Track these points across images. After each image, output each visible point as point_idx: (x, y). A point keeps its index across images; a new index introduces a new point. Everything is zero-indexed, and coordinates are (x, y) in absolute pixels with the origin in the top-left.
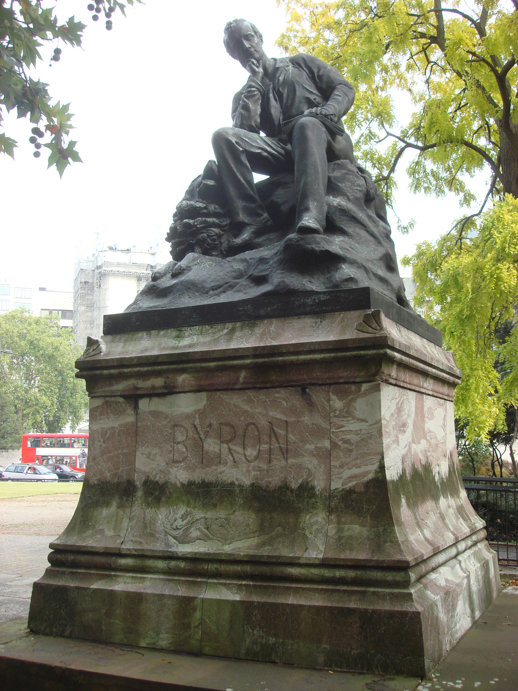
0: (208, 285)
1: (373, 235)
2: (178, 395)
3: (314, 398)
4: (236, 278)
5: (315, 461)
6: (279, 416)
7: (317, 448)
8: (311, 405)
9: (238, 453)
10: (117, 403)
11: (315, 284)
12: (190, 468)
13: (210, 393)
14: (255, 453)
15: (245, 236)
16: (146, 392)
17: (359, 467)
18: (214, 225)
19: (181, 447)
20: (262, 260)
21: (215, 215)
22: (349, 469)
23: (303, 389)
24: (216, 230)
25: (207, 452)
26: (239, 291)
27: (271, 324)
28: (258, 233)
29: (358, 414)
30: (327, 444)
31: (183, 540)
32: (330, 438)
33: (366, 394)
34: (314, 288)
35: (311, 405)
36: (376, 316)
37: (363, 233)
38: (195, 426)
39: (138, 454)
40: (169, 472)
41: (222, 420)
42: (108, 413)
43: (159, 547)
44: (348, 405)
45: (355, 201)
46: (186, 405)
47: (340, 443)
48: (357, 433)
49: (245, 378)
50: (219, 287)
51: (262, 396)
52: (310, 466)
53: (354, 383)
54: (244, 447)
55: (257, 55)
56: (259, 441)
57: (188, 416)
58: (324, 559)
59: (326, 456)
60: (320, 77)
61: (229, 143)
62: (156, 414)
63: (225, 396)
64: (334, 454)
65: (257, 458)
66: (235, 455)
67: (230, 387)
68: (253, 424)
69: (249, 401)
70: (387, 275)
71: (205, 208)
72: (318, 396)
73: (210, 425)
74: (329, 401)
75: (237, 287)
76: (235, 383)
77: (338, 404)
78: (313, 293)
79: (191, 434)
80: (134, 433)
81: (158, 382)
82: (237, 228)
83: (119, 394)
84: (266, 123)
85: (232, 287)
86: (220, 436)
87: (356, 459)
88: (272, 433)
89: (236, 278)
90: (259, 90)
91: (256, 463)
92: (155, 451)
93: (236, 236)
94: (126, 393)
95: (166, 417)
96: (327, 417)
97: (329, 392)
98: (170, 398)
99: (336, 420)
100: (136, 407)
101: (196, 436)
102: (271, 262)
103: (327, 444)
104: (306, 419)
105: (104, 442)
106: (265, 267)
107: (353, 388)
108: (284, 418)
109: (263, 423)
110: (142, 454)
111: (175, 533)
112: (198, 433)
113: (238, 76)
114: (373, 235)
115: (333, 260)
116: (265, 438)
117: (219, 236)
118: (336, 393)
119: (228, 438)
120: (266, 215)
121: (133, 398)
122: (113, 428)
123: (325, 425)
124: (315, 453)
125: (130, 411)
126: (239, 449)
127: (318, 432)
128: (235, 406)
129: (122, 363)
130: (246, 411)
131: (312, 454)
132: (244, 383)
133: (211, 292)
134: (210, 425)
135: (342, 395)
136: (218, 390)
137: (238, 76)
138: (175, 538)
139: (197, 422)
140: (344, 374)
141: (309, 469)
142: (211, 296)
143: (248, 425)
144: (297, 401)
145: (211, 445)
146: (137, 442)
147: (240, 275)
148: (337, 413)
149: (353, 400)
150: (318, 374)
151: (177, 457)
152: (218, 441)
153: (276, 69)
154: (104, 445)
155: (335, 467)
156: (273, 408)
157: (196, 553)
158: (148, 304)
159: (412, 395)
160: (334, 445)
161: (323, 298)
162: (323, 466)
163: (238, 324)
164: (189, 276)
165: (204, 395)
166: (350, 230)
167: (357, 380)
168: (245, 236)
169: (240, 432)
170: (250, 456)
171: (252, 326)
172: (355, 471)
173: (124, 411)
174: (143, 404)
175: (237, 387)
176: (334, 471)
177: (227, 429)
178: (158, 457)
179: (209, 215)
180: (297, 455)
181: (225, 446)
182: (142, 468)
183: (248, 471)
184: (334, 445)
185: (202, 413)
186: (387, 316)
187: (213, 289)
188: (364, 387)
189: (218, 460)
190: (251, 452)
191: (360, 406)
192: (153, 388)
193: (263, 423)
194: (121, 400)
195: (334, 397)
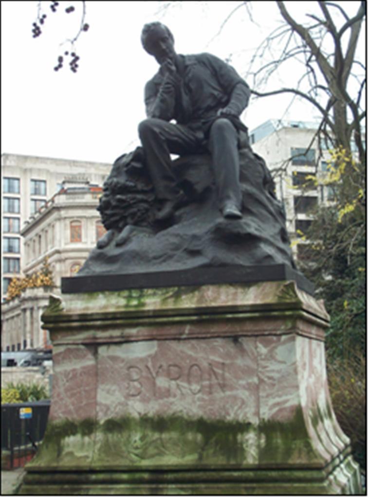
0: (151, 255)
1: (271, 213)
2: (135, 344)
3: (245, 346)
4: (173, 250)
5: (247, 393)
6: (217, 359)
7: (249, 384)
8: (243, 351)
9: (185, 388)
10: (78, 350)
11: (242, 259)
12: (145, 400)
13: (160, 342)
14: (198, 388)
15: (167, 210)
16: (105, 341)
17: (280, 396)
18: (142, 201)
19: (136, 384)
20: (195, 237)
21: (143, 192)
22: (274, 398)
23: (235, 339)
24: (145, 205)
25: (159, 388)
26: (178, 261)
27: (208, 289)
28: (177, 207)
29: (279, 358)
30: (255, 380)
31: (142, 457)
32: (258, 376)
33: (285, 342)
34: (241, 262)
35: (243, 351)
36: (291, 286)
37: (264, 212)
38: (147, 367)
39: (99, 391)
40: (127, 405)
41: (171, 363)
42: (70, 358)
43: (123, 463)
44: (271, 351)
45: (256, 185)
46: (140, 350)
47: (266, 379)
48: (278, 372)
49: (190, 330)
50: (160, 257)
51: (203, 344)
52: (243, 397)
53: (275, 335)
54: (189, 382)
55: (171, 55)
56: (201, 378)
57: (142, 360)
58: (259, 465)
59: (255, 389)
60: (222, 76)
61: (154, 132)
62: (114, 359)
63: (174, 345)
64: (261, 387)
65: (199, 391)
66: (183, 390)
67: (177, 337)
68: (196, 365)
69: (193, 347)
70: (282, 245)
71: (135, 186)
72: (248, 344)
73: (161, 367)
74: (256, 347)
75: (175, 258)
76: (181, 334)
77: (263, 350)
78: (241, 266)
79: (144, 374)
80: (96, 374)
81: (116, 333)
82: (160, 203)
83: (80, 342)
84: (178, 113)
85: (170, 257)
86: (168, 375)
87: (278, 391)
88: (212, 372)
89: (173, 250)
90: (173, 86)
91: (199, 395)
92: (114, 387)
93: (159, 210)
94: (87, 341)
95: (123, 361)
96: (255, 360)
97: (256, 341)
98: (124, 346)
99: (263, 363)
100: (95, 353)
101: (149, 376)
102: (203, 239)
103: (255, 380)
104: (239, 362)
105: (67, 381)
106: (198, 243)
107: (275, 338)
108: (221, 360)
109: (205, 364)
110: (103, 390)
111: (137, 452)
112: (151, 373)
113: (151, 67)
114: (271, 213)
115: (253, 240)
116: (206, 376)
117: (147, 210)
118: (261, 342)
119: (177, 376)
120: (182, 192)
121: (93, 346)
122: (74, 370)
123: (254, 366)
124: (247, 386)
125: (90, 356)
126: (185, 385)
127: (249, 371)
128: (182, 352)
129: (84, 318)
130: (190, 357)
131: (244, 387)
132: (189, 334)
133: (155, 261)
134: (161, 367)
135: (266, 344)
136: (166, 339)
137: (151, 67)
138: (137, 455)
139: (150, 364)
140: (268, 327)
141: (241, 398)
142: (154, 264)
143: (192, 366)
144: (230, 347)
145: (162, 382)
146: (97, 381)
147: (177, 248)
148: (263, 357)
149: (275, 348)
150: (249, 327)
151: (132, 392)
152: (167, 379)
153: (186, 67)
154: (67, 384)
155: (263, 397)
156: (209, 353)
157: (157, 466)
158: (99, 269)
159: (307, 340)
160: (261, 381)
161: (249, 270)
162: (253, 397)
163: (183, 288)
164: (132, 246)
165: (155, 343)
166: (254, 210)
167: (278, 332)
168: (167, 210)
169: (186, 372)
170: (195, 390)
171: (193, 291)
172: (277, 400)
173: (85, 356)
174: (102, 350)
175: (184, 336)
176: (262, 400)
177: (176, 369)
178: (117, 393)
179: (138, 192)
180: (232, 388)
181: (173, 382)
182: (104, 402)
183: (194, 402)
184: (261, 381)
185: (154, 357)
186: (301, 289)
187: (155, 258)
188: (284, 338)
189: (168, 393)
190: (195, 387)
191: (281, 351)
192: (111, 337)
193: (205, 364)
194: (82, 347)
195: (260, 345)
